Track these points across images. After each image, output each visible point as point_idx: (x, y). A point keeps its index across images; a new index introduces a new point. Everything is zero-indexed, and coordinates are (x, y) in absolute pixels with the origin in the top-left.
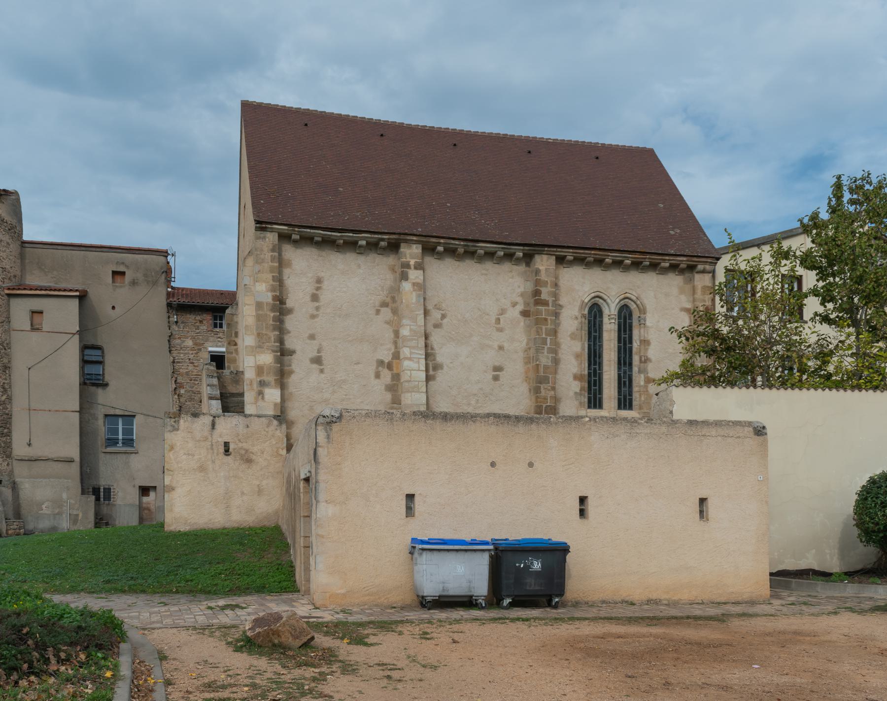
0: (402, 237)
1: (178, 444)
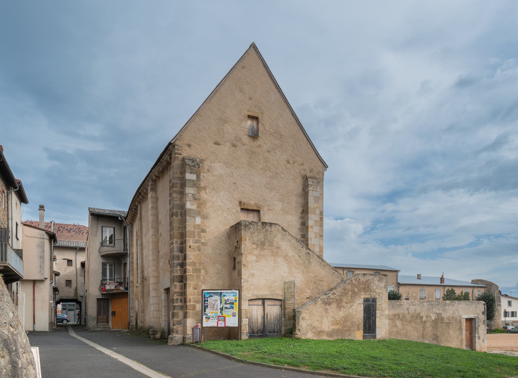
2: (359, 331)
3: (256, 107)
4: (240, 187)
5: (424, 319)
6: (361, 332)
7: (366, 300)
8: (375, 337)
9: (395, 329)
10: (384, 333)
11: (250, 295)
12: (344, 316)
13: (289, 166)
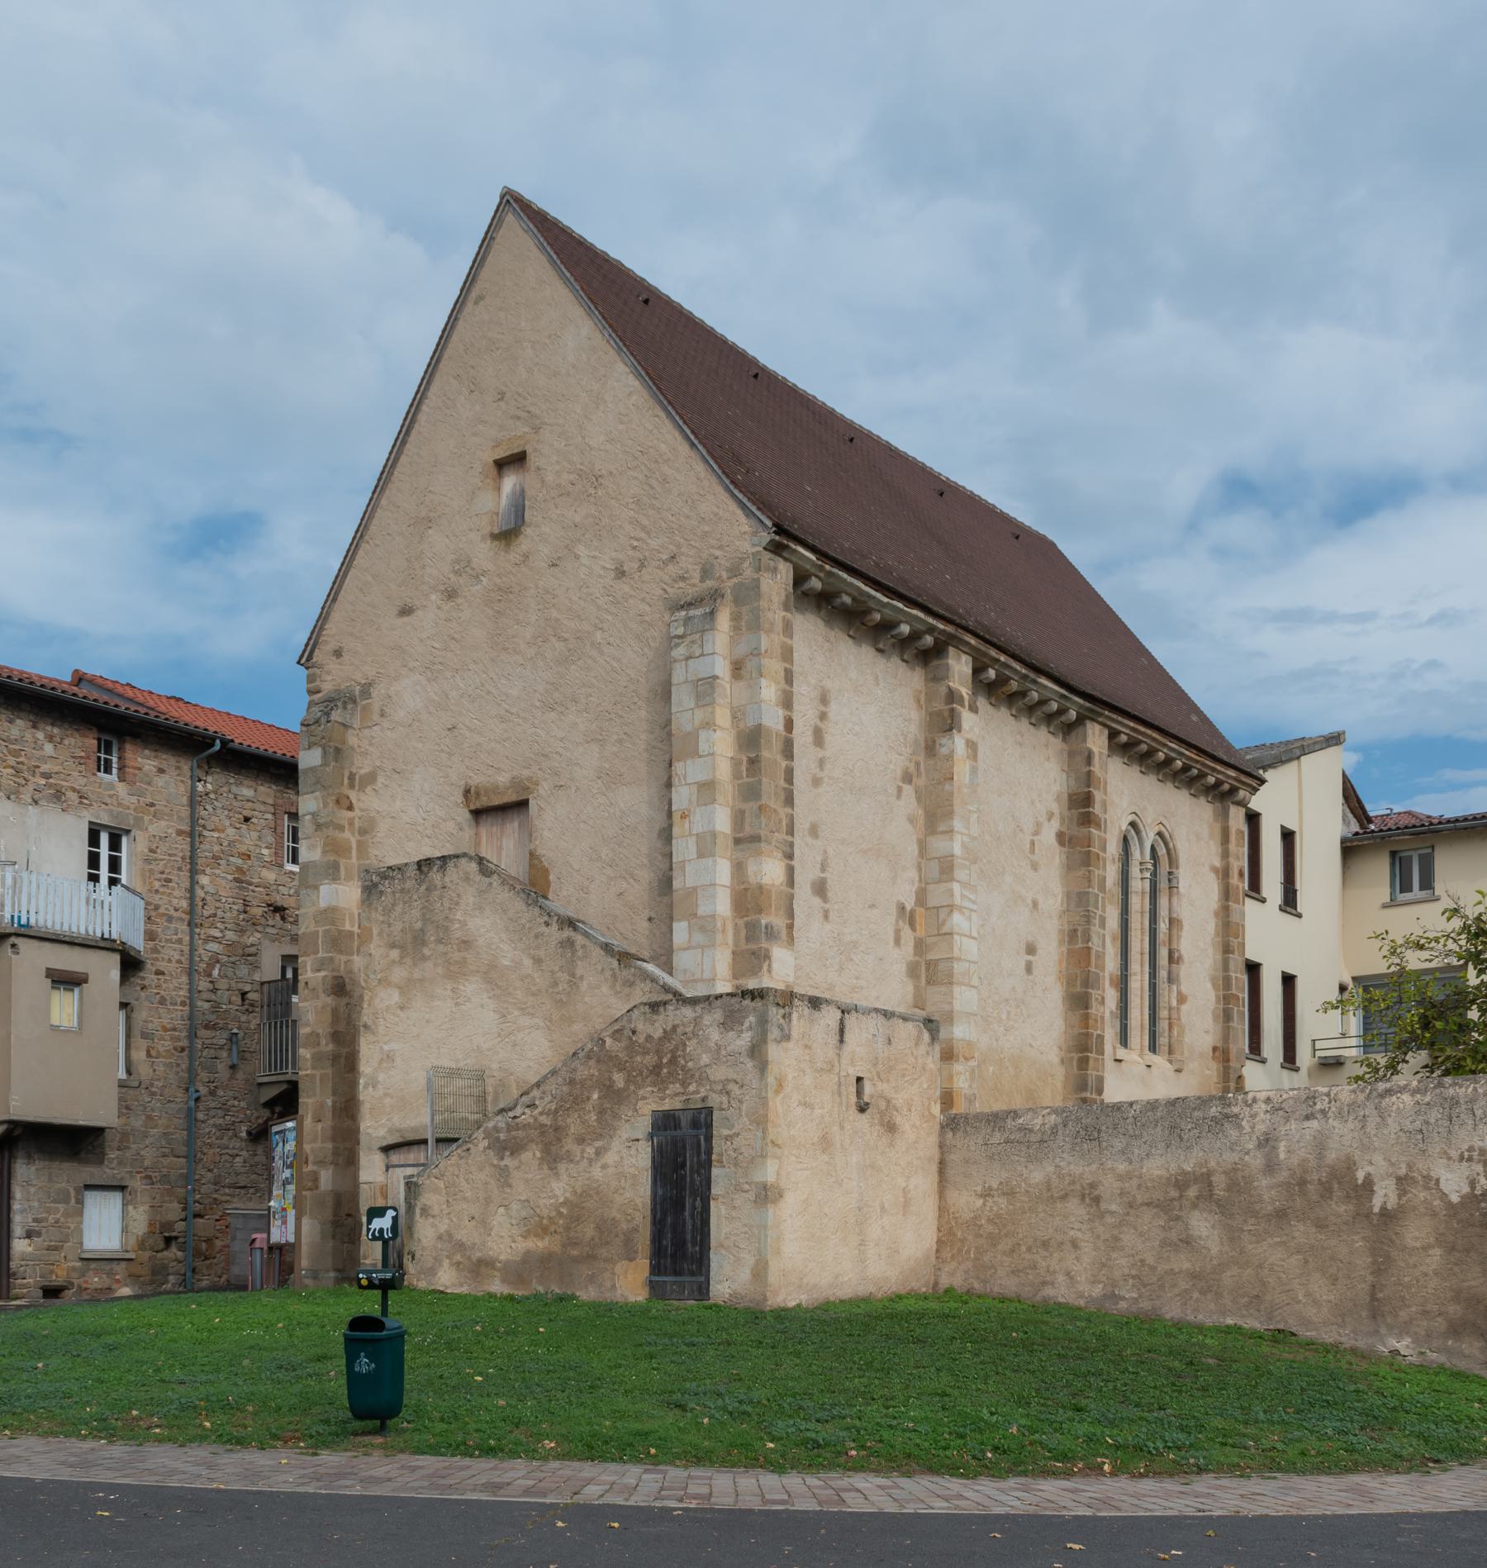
0: (961, 634)
1: (790, 1077)
2: (631, 1260)
3: (519, 418)
4: (468, 734)
5: (1384, 1195)
6: (643, 1265)
7: (665, 1122)
8: (703, 1291)
9: (1183, 1262)
10: (748, 1271)
11: (382, 1132)
12: (572, 1198)
13: (624, 587)
